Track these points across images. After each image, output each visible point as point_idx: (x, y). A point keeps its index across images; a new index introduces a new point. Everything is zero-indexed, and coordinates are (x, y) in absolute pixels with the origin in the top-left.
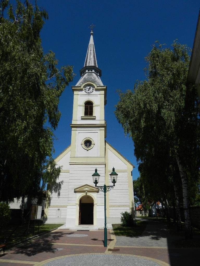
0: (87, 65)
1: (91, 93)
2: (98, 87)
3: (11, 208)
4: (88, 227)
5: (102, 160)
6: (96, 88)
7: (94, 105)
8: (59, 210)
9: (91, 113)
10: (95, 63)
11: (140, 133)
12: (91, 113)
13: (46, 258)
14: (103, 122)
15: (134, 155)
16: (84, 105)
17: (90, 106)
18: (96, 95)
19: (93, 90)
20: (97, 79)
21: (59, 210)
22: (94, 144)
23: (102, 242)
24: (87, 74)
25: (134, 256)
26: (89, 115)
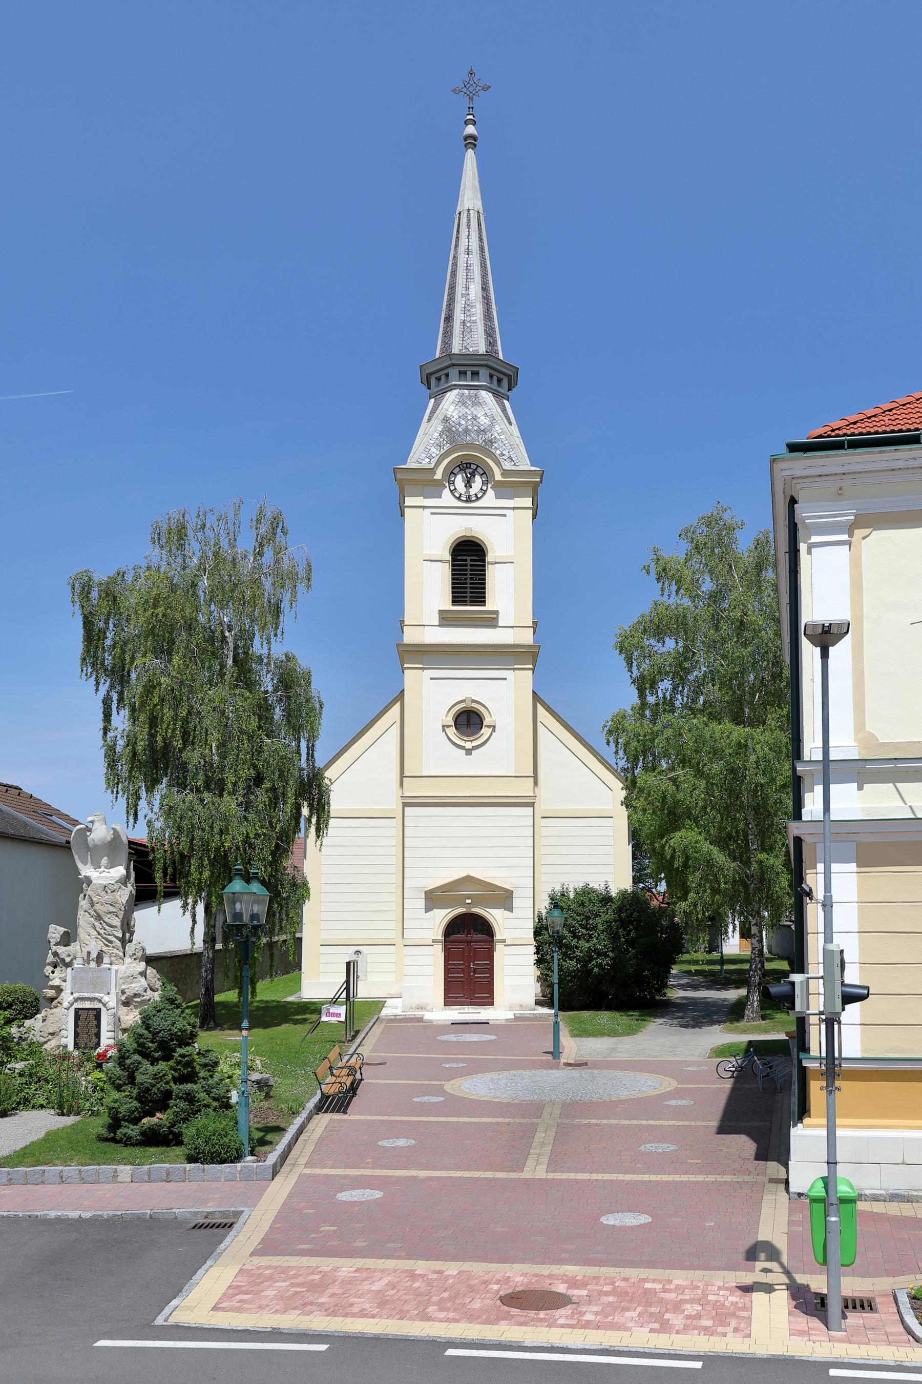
0: (456, 350)
1: (478, 499)
2: (505, 473)
5: (524, 788)
6: (498, 477)
7: (489, 558)
9: (479, 597)
10: (491, 343)
11: (670, 758)
12: (480, 579)
14: (526, 637)
16: (449, 558)
18: (498, 513)
22: (494, 727)
23: (847, 1007)
24: (455, 392)
25: (512, 1072)
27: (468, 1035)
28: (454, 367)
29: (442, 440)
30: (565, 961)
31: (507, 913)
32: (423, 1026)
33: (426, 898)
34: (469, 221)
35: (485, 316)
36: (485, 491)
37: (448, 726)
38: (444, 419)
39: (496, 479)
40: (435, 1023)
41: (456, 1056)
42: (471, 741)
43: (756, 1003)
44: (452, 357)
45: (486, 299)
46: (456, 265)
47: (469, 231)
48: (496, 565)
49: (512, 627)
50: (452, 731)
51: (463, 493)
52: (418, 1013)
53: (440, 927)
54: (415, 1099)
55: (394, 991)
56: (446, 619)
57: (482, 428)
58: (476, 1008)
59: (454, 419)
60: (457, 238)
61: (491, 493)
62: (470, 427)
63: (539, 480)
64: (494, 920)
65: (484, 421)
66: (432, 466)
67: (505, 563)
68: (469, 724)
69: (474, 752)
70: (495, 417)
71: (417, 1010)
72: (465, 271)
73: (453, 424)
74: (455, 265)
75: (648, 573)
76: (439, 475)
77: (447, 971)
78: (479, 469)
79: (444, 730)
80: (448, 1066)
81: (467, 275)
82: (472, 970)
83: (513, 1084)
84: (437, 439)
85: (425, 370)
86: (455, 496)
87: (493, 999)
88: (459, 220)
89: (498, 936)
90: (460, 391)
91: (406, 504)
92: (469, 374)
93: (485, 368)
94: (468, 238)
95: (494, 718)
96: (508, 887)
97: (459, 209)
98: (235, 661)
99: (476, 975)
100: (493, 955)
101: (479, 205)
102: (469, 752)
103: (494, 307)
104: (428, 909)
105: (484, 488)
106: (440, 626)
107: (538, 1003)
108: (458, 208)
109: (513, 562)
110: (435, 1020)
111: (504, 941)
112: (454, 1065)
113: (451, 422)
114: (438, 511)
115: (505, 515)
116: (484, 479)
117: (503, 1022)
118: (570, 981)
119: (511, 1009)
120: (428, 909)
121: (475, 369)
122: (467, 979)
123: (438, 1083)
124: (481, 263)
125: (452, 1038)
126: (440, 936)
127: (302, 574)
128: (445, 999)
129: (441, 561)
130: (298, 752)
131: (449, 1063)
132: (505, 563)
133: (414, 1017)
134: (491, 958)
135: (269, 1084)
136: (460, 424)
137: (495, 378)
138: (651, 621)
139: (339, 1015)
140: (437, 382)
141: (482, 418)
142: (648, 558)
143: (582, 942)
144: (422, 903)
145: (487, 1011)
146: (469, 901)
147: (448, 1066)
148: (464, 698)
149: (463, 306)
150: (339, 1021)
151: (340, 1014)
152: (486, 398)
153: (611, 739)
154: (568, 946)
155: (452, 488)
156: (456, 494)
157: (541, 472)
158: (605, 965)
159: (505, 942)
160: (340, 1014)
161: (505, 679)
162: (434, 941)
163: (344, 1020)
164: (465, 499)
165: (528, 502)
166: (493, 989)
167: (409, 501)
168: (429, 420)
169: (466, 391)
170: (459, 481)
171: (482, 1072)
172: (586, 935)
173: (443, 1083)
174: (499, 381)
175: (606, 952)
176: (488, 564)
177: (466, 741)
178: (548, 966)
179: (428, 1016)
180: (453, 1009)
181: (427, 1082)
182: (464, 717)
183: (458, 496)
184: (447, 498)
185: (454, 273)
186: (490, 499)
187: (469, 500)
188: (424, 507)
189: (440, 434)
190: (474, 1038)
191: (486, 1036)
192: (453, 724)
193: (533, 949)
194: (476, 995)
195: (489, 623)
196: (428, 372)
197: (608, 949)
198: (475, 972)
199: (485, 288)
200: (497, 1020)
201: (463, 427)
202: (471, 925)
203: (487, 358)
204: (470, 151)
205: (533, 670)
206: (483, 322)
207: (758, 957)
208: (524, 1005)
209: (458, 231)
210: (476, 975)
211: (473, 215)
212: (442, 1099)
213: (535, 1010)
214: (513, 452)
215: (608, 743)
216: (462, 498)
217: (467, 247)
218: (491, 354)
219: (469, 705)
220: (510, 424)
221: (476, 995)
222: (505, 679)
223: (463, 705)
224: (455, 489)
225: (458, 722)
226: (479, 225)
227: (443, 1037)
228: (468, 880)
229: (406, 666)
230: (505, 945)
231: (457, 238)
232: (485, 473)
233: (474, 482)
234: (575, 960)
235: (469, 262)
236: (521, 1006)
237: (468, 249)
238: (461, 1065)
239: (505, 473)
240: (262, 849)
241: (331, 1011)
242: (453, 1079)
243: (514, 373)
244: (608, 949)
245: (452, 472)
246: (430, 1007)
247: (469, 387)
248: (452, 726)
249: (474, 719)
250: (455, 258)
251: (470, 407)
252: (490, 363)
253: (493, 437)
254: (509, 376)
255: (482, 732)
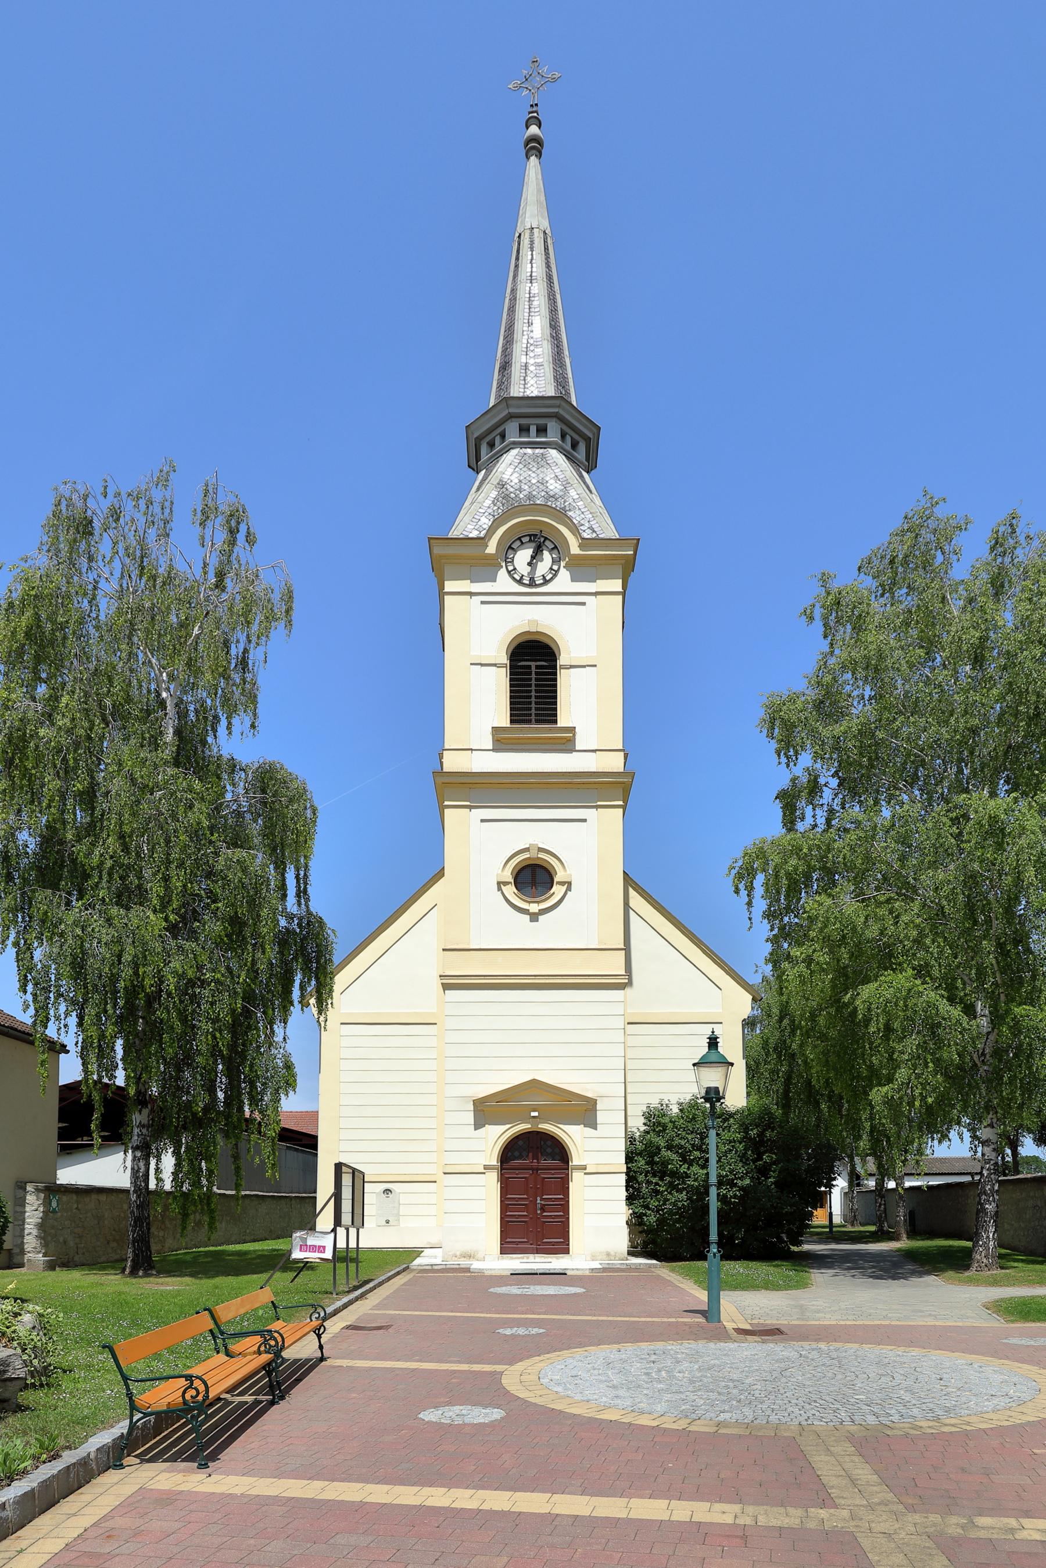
1: (546, 582)
2: (585, 543)
3: (1024, 1155)
4: (549, 1260)
6: (575, 549)
7: (562, 660)
8: (387, 1191)
13: (768, 1286)
14: (615, 763)
15: (309, 787)
16: (504, 659)
17: (537, 667)
18: (575, 600)
19: (555, 567)
20: (580, 491)
21: (387, 1191)
22: (570, 884)
24: (514, 452)
26: (538, 722)
27: (538, 1287)
28: (513, 419)
29: (496, 508)
30: (670, 1193)
31: (589, 1131)
32: (469, 1277)
33: (476, 1111)
34: (532, 242)
35: (554, 360)
36: (556, 571)
37: (506, 883)
38: (498, 484)
39: (572, 552)
40: (487, 1273)
41: (523, 1316)
42: (538, 902)
43: (991, 1243)
44: (510, 402)
45: (556, 339)
46: (515, 299)
47: (532, 255)
48: (572, 670)
49: (594, 751)
50: (510, 890)
51: (526, 574)
52: (464, 1263)
53: (494, 1152)
54: (429, 1416)
55: (434, 1240)
56: (502, 741)
57: (552, 493)
58: (545, 1258)
59: (512, 484)
60: (517, 266)
61: (564, 574)
62: (534, 493)
63: (632, 553)
64: (570, 1140)
65: (554, 486)
66: (482, 535)
67: (584, 667)
68: (534, 883)
69: (541, 918)
70: (569, 481)
71: (463, 1259)
72: (527, 303)
73: (512, 490)
74: (514, 299)
75: (811, 618)
76: (492, 548)
77: (505, 1208)
78: (547, 543)
79: (500, 889)
80: (508, 1332)
81: (530, 308)
82: (539, 1206)
83: (663, 1373)
84: (489, 507)
85: (473, 434)
86: (514, 579)
87: (568, 1245)
88: (519, 244)
89: (576, 1161)
90: (521, 451)
91: (446, 590)
92: (533, 429)
93: (555, 419)
94: (531, 262)
95: (568, 872)
96: (590, 1095)
97: (519, 230)
98: (178, 732)
99: (545, 1214)
100: (568, 1188)
101: (545, 224)
102: (534, 917)
103: (566, 352)
104: (478, 1126)
105: (555, 567)
106: (493, 750)
107: (630, 1253)
108: (518, 228)
109: (595, 666)
110: (486, 1270)
111: (583, 1168)
112: (521, 1331)
113: (509, 487)
114: (491, 599)
115: (584, 604)
116: (554, 556)
117: (587, 1273)
118: (678, 1221)
119: (594, 1259)
120: (478, 1126)
121: (541, 421)
122: (531, 1218)
123: (487, 1368)
124: (549, 297)
125: (515, 1290)
126: (494, 1161)
127: (280, 609)
128: (501, 1244)
129: (495, 665)
130: (283, 887)
131: (512, 1327)
132: (584, 667)
133: (457, 1267)
134: (565, 1191)
135: (8, 1375)
136: (520, 490)
137: (568, 439)
138: (818, 683)
139: (322, 1249)
140: (489, 449)
141: (552, 481)
142: (811, 593)
143: (695, 1169)
144: (470, 1118)
145: (561, 1260)
146: (535, 1114)
147: (508, 1332)
148: (527, 846)
149: (525, 346)
150: (322, 1259)
151: (324, 1247)
152: (557, 458)
153: (742, 886)
154: (674, 1174)
155: (510, 568)
156: (516, 576)
157: (635, 541)
158: (731, 1197)
159: (585, 1169)
160: (324, 1247)
161: (585, 820)
162: (486, 1167)
163: (330, 1257)
164: (528, 582)
165: (616, 585)
166: (568, 1232)
167: (450, 586)
168: (478, 489)
169: (529, 451)
170: (523, 556)
171: (581, 1345)
172: (700, 1159)
173: (499, 1368)
174: (574, 445)
175: (733, 1180)
176: (560, 668)
177: (530, 902)
178: (644, 1202)
179: (476, 1265)
180: (512, 1258)
181: (465, 1367)
182: (528, 873)
183: (518, 578)
184: (503, 582)
185: (512, 309)
186: (564, 581)
187: (532, 583)
188: (471, 594)
189: (493, 501)
190: (551, 1290)
191: (567, 1288)
192: (513, 881)
193: (622, 1179)
194: (545, 1240)
195: (563, 747)
196: (476, 435)
197: (735, 1175)
198: (543, 1210)
199: (554, 325)
200: (577, 1269)
201: (525, 493)
202: (538, 1148)
203: (558, 402)
204: (533, 159)
205: (624, 808)
206: (551, 366)
207: (995, 1173)
208: (612, 1253)
209: (517, 259)
210: (545, 1214)
211: (538, 235)
212: (496, 1414)
213: (627, 1260)
214: (595, 522)
215: (737, 891)
216: (524, 582)
217: (529, 274)
218: (561, 399)
219: (533, 854)
220: (591, 492)
221: (545, 1240)
222: (585, 820)
223: (526, 855)
224: (515, 569)
225: (519, 880)
226: (546, 249)
227: (499, 1289)
228: (534, 1086)
229: (446, 803)
230: (585, 1174)
231: (517, 266)
232: (556, 547)
233: (542, 560)
234: (684, 1193)
235: (532, 292)
236: (608, 1254)
237: (531, 276)
238: (535, 1331)
239: (585, 543)
240: (212, 1004)
241: (309, 1243)
242: (521, 1360)
243: (594, 434)
244: (735, 1175)
245: (510, 547)
246: (480, 1255)
247: (533, 445)
248: (511, 883)
249: (541, 876)
250: (514, 291)
251: (534, 469)
252: (562, 412)
253: (567, 503)
254: (588, 440)
255: (552, 892)
